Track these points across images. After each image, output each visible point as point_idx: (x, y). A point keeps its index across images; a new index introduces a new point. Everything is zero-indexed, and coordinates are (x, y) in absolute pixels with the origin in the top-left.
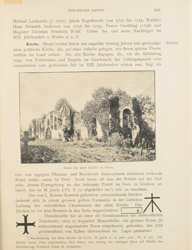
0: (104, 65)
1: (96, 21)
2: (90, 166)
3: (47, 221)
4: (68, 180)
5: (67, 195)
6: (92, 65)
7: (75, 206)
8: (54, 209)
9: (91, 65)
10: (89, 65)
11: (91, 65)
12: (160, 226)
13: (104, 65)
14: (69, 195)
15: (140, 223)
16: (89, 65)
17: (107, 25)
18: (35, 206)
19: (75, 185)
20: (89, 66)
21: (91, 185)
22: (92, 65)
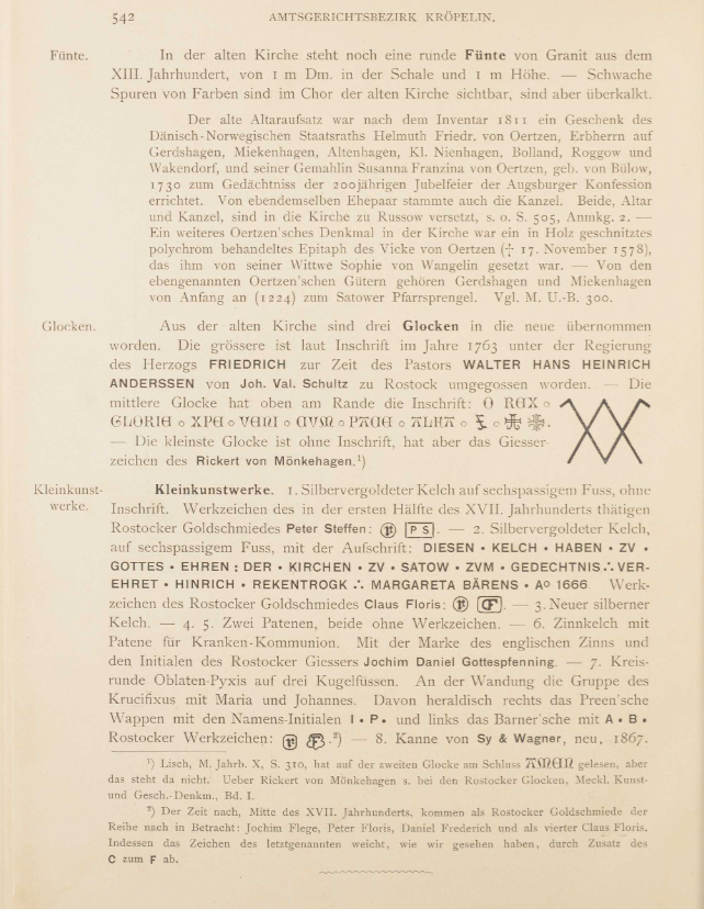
0: (535, 511)
1: (141, 95)
2: (422, 483)
3: (516, 721)
4: (211, 170)
5: (117, 738)
6: (134, 76)
7: (608, 327)
8: (444, 822)
9: (128, 77)
10: (122, 76)
11: (128, 77)
12: (464, 218)
13: (535, 511)
14: (126, 529)
15: (322, 274)
16: (122, 74)
17: (409, 362)
18: (205, 663)
19: (554, 702)
20: (123, 77)
21: (309, 405)
22: (134, 76)
